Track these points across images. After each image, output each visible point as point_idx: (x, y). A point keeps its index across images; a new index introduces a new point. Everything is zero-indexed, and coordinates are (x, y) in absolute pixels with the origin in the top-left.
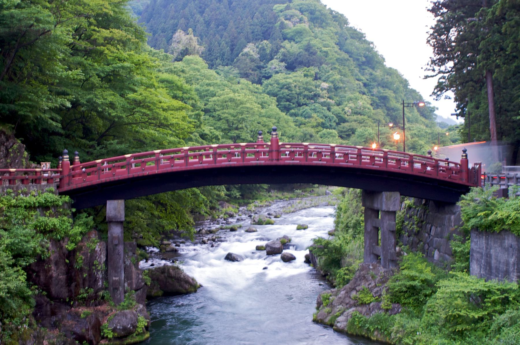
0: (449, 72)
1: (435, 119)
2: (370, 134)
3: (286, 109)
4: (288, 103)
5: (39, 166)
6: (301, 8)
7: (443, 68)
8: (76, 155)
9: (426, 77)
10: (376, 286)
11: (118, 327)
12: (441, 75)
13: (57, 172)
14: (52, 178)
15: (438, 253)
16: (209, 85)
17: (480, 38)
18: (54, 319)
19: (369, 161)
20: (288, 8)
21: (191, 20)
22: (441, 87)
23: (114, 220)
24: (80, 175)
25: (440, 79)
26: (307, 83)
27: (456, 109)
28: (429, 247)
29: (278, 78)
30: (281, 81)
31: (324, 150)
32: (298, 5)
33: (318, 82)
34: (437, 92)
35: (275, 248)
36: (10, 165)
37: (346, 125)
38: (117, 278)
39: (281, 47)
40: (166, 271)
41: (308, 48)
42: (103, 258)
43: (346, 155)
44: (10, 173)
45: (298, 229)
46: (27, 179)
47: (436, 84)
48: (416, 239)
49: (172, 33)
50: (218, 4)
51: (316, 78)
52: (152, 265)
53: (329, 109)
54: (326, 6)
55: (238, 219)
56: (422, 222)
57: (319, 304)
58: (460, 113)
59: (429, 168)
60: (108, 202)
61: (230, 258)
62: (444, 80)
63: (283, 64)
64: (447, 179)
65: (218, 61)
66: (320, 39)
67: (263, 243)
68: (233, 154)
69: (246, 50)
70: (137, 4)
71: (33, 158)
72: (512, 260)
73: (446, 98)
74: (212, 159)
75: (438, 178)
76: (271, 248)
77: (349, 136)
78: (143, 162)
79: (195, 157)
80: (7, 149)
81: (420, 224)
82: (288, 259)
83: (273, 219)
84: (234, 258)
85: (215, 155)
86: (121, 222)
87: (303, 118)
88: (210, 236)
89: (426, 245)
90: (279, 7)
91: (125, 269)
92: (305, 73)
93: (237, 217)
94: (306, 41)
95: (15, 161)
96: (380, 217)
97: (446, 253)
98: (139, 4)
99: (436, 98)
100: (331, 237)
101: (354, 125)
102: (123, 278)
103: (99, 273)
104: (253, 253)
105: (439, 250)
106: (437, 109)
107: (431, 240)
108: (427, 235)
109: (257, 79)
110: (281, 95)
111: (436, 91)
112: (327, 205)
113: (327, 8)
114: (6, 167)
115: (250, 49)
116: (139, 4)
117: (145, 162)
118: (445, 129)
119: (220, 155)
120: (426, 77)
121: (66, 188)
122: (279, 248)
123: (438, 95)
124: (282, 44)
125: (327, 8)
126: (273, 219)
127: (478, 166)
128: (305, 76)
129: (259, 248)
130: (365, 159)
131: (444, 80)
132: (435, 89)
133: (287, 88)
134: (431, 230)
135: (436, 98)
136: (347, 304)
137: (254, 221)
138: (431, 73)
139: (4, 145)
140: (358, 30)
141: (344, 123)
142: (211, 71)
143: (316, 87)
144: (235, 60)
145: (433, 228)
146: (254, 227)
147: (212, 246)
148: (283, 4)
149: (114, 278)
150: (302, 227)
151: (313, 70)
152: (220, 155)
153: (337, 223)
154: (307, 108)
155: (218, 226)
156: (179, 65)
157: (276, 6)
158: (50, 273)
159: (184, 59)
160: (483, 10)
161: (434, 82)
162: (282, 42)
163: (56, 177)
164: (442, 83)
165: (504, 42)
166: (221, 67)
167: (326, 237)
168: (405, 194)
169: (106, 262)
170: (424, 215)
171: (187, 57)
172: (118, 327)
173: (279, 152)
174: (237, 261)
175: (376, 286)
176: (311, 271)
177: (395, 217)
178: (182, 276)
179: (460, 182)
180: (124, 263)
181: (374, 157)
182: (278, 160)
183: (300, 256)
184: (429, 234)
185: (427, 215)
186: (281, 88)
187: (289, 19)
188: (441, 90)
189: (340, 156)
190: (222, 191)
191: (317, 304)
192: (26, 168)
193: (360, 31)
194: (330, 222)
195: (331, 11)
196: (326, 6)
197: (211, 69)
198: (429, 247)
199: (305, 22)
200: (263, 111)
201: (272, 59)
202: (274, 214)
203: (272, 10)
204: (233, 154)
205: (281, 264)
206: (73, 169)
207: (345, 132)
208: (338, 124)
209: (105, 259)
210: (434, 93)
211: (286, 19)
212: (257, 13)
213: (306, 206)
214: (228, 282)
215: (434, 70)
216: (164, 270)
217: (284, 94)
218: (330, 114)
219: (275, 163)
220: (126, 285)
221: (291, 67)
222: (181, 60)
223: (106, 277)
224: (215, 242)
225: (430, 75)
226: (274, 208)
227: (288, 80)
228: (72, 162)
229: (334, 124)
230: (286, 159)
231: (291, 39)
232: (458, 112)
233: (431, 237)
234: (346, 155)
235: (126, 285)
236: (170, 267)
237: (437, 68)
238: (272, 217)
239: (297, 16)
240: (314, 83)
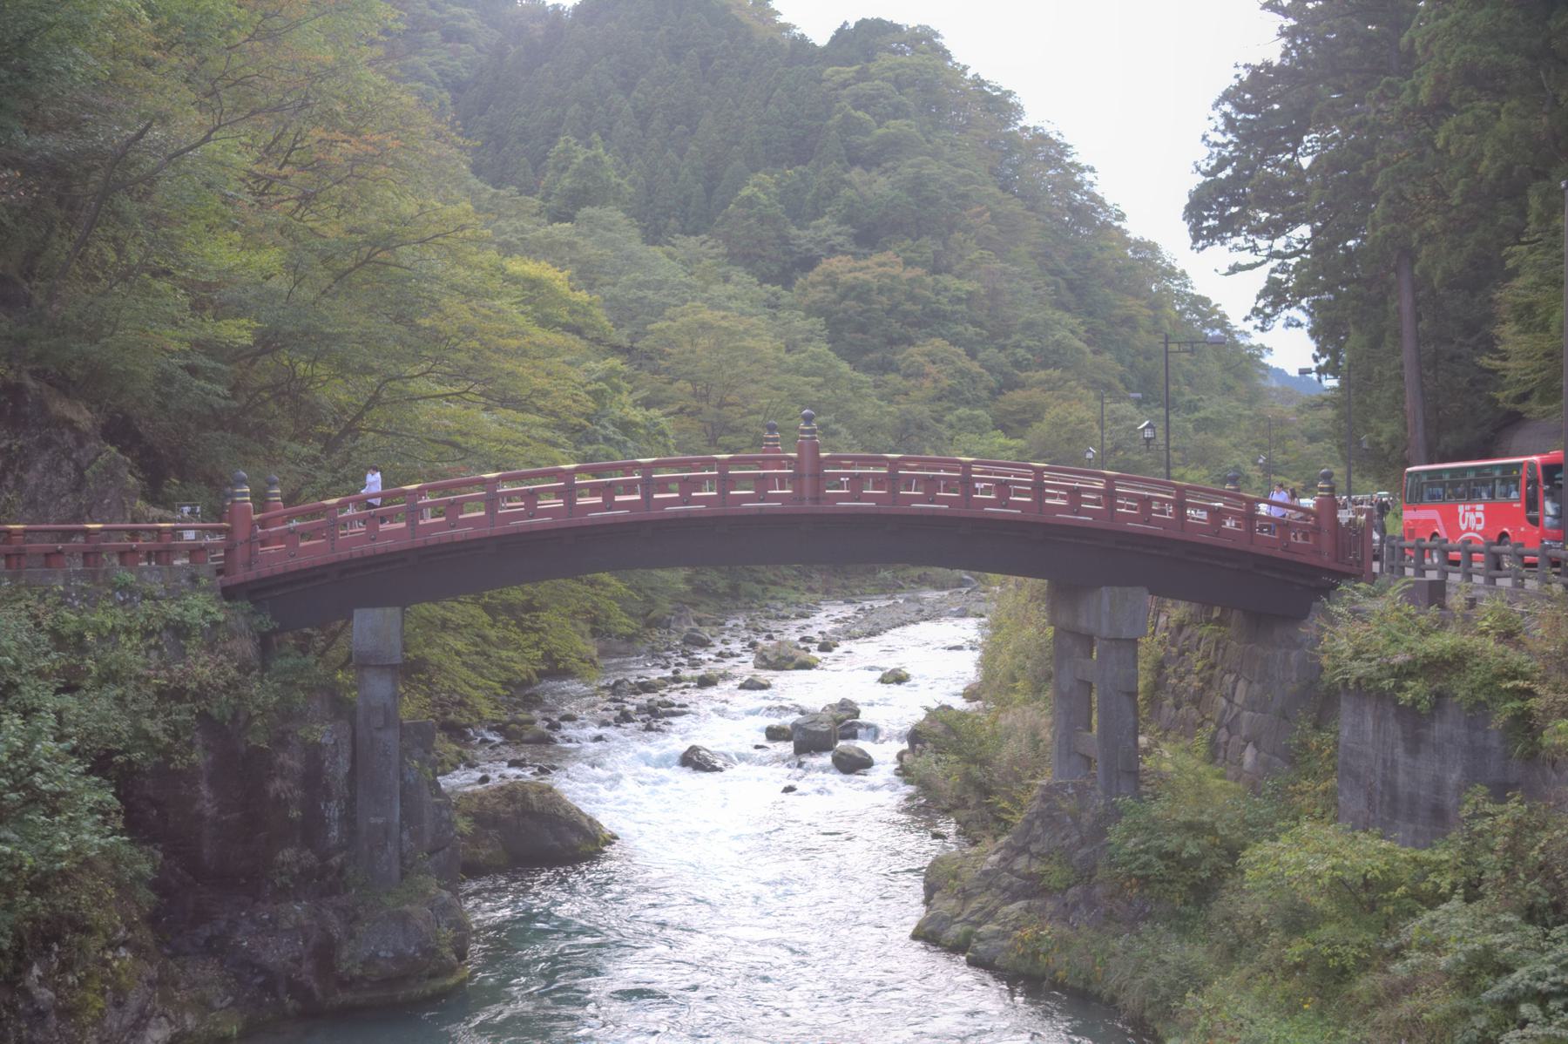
0: (1296, 253)
1: (1264, 377)
2: (1082, 421)
3: (853, 354)
4: (860, 336)
5: (169, 514)
6: (897, 76)
7: (1279, 244)
8: (272, 484)
9: (1235, 269)
10: (1083, 843)
11: (382, 954)
12: (1275, 262)
13: (219, 531)
14: (202, 549)
15: (1255, 751)
16: (641, 285)
17: (1378, 162)
18: (206, 931)
19: (1063, 503)
20: (863, 76)
21: (599, 108)
22: (1276, 295)
23: (373, 663)
24: (280, 538)
25: (1273, 271)
26: (912, 281)
27: (1317, 354)
28: (1231, 735)
29: (833, 269)
30: (843, 278)
31: (1012, 478)
32: (890, 69)
33: (947, 280)
34: (1265, 306)
35: (816, 733)
36: (89, 513)
37: (1018, 396)
38: (380, 821)
39: (844, 182)
40: (520, 796)
41: (917, 186)
42: (344, 766)
43: (1003, 488)
44: (87, 532)
45: (882, 681)
46: (133, 551)
47: (1263, 285)
48: (1194, 713)
49: (549, 142)
50: (674, 65)
51: (936, 270)
52: (484, 780)
53: (972, 355)
54: (965, 68)
55: (720, 654)
56: (1213, 667)
57: (931, 890)
58: (1328, 363)
59: (1229, 524)
60: (356, 611)
61: (695, 761)
62: (1283, 277)
63: (846, 228)
64: (1278, 553)
65: (673, 222)
66: (949, 160)
67: (788, 720)
68: (698, 483)
69: (745, 192)
70: (451, 63)
71: (154, 495)
72: (1454, 776)
73: (1290, 325)
74: (992, 497)
75: (1253, 549)
76: (806, 732)
77: (1024, 423)
78: (451, 504)
79: (594, 490)
80: (79, 469)
81: (1206, 674)
82: (853, 765)
83: (816, 654)
84: (706, 760)
85: (649, 486)
86: (393, 667)
87: (900, 378)
88: (643, 699)
89: (1224, 730)
90: (838, 73)
91: (402, 793)
92: (908, 254)
93: (721, 648)
94: (912, 166)
95: (102, 501)
96: (1095, 656)
97: (1274, 754)
98: (458, 63)
99: (1260, 325)
100: (973, 706)
101: (1036, 395)
102: (397, 820)
103: (333, 804)
104: (757, 747)
105: (1256, 745)
106: (1270, 350)
107: (1237, 716)
108: (1224, 702)
109: (775, 269)
110: (840, 315)
111: (1261, 303)
112: (963, 614)
113: (970, 74)
114: (78, 518)
115: (760, 187)
116: (458, 63)
117: (458, 506)
118: (1292, 407)
119: (663, 485)
120: (1235, 269)
121: (241, 575)
122: (828, 733)
123: (1268, 316)
124: (846, 176)
125: (970, 74)
126: (816, 654)
127: (1364, 517)
128: (908, 263)
129: (774, 734)
130: (1053, 496)
131: (1283, 277)
132: (1259, 298)
133: (859, 298)
134: (1234, 689)
135: (1260, 325)
136: (1005, 890)
137: (764, 658)
138: (1247, 258)
139: (69, 458)
140: (1054, 136)
141: (1011, 389)
142: (652, 249)
143: (938, 294)
144: (719, 219)
145: (1241, 685)
146: (765, 675)
147: (649, 728)
148: (851, 65)
149: (373, 820)
150: (896, 678)
151: (929, 246)
152: (663, 485)
153: (986, 664)
154: (912, 350)
155: (668, 674)
156: (562, 230)
157: (829, 71)
158: (198, 807)
159: (579, 215)
160: (1389, 85)
161: (1258, 279)
162: (846, 170)
163: (215, 547)
164: (1279, 282)
165: (1444, 171)
166: (680, 240)
167: (959, 704)
168: (1165, 589)
169: (352, 773)
170: (1217, 649)
171: (587, 211)
172: (382, 954)
173: (819, 479)
174: (714, 769)
175: (1083, 843)
176: (910, 798)
177: (1135, 656)
178: (562, 812)
179: (1315, 561)
180: (402, 777)
181: (1079, 491)
182: (816, 500)
183: (885, 754)
184: (1230, 701)
185: (1225, 650)
186: (844, 297)
187: (865, 108)
188: (1275, 305)
189: (986, 490)
190: (676, 578)
191: (925, 888)
192: (134, 521)
193: (1060, 138)
194: (967, 667)
195: (979, 82)
196: (965, 68)
197: (654, 243)
198: (1231, 735)
199: (907, 116)
200: (790, 359)
201: (818, 214)
202: (819, 638)
203: (820, 81)
204: (698, 483)
205: (835, 779)
206: (263, 523)
207: (1012, 413)
208: (995, 393)
209: (347, 769)
210: (1256, 311)
211: (857, 108)
212: (779, 90)
213: (904, 617)
214: (873, 639)
215: (1255, 249)
216: (512, 794)
217: (850, 312)
218: (975, 367)
219: (808, 506)
220: (405, 837)
221: (868, 237)
222: (570, 218)
223: (349, 819)
224: (656, 716)
225: (1243, 263)
226: (824, 620)
227: (860, 275)
228: (261, 499)
229: (985, 394)
230: (839, 497)
231: (870, 161)
232: (1323, 361)
233: (1236, 709)
234: (1003, 488)
235: (405, 837)
236: (532, 784)
237: (1263, 243)
238: (814, 647)
239: (887, 98)
240: (929, 280)
